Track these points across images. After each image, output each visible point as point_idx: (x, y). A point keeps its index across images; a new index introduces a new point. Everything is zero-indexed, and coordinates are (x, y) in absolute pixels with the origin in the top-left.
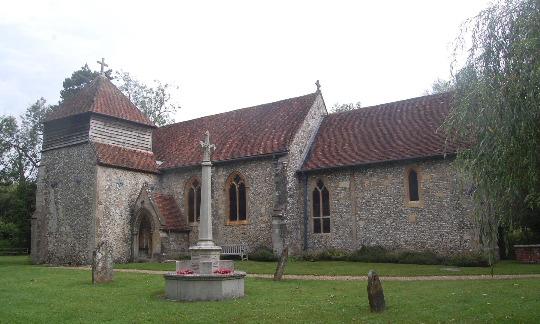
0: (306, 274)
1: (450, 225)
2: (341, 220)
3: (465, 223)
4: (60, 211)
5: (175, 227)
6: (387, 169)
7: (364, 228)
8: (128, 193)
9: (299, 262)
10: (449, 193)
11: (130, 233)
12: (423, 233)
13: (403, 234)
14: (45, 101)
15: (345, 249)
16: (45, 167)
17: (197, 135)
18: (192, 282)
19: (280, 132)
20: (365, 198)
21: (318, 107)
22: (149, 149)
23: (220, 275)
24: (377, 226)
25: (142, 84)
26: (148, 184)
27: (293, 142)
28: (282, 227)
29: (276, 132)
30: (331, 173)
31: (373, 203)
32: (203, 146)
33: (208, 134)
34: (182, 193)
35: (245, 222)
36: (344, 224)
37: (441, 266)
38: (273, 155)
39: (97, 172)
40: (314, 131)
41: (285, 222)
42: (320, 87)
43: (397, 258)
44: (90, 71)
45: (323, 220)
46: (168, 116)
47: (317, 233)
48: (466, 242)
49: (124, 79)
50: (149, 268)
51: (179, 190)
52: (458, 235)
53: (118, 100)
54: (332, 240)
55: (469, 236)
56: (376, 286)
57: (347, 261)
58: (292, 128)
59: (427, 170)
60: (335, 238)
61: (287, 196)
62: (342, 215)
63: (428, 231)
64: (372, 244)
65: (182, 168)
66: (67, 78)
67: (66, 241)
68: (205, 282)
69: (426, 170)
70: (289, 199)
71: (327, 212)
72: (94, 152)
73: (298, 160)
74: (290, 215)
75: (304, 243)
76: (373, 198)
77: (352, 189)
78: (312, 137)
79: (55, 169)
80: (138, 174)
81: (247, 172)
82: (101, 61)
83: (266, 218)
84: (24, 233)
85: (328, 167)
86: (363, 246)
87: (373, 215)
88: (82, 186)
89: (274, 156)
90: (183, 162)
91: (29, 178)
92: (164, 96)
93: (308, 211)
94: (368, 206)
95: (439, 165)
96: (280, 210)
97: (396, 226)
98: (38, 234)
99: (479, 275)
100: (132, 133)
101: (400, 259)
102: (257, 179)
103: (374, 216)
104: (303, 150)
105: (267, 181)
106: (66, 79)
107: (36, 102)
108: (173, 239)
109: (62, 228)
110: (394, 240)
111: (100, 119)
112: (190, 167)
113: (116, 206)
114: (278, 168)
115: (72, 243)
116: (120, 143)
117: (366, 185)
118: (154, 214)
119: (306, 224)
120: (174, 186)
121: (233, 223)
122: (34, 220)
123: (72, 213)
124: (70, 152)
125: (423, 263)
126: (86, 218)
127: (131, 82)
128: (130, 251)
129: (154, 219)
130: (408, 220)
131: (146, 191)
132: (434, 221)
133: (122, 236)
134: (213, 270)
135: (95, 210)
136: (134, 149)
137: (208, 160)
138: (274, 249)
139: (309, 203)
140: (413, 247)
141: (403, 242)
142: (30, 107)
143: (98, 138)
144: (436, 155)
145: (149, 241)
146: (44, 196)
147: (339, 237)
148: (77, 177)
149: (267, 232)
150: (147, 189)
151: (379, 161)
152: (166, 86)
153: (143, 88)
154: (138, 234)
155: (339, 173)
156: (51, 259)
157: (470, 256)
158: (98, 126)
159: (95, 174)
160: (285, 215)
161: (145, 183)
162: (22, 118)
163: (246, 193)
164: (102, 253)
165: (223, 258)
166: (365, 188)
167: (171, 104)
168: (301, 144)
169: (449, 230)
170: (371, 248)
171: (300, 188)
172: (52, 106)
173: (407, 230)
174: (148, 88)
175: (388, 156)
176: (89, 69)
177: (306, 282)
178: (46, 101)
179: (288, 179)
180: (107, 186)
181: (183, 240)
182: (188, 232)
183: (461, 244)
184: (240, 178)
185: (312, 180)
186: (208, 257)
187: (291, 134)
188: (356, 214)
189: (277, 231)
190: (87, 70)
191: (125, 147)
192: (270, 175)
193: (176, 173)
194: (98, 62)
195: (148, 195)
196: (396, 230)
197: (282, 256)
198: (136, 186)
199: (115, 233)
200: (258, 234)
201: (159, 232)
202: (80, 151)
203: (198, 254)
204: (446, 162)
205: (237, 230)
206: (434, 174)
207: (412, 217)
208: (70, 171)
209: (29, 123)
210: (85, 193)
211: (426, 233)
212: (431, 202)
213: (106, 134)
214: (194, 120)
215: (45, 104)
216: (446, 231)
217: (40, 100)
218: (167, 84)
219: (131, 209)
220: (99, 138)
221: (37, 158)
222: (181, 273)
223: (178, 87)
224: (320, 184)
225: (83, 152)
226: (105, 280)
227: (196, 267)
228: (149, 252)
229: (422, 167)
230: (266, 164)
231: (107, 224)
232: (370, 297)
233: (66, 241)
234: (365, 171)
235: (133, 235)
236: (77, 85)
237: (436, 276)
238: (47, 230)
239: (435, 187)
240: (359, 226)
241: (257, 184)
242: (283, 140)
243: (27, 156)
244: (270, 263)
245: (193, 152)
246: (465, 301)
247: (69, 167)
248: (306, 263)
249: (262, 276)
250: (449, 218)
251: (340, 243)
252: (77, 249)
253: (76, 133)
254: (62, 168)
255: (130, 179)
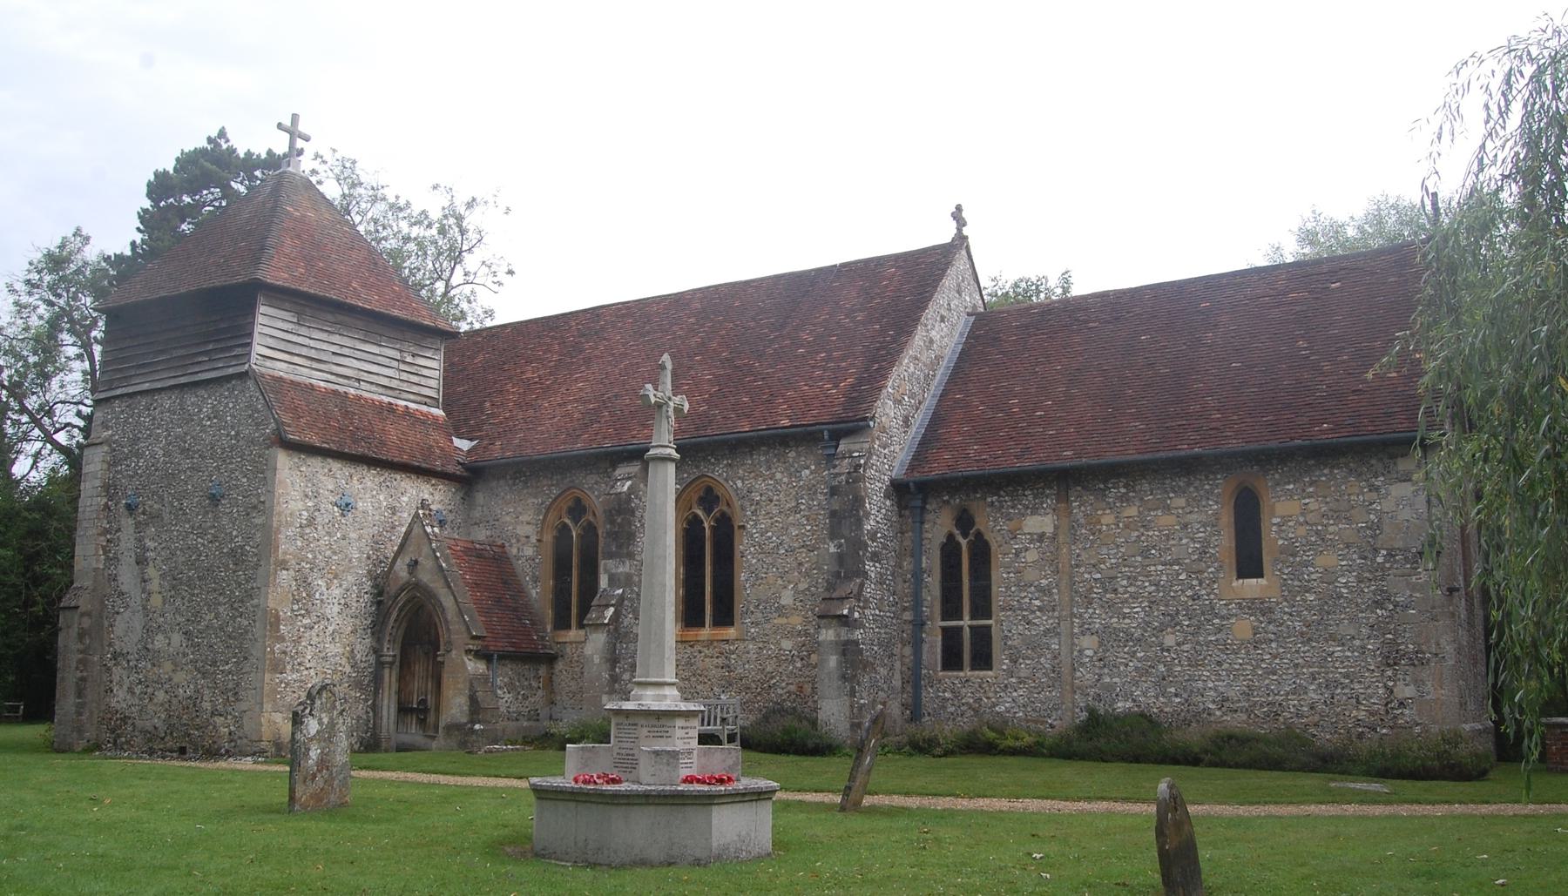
0: (928, 792)
1: (1356, 654)
2: (1027, 632)
3: (1402, 647)
4: (154, 585)
5: (513, 644)
6: (1167, 482)
7: (1095, 658)
8: (367, 537)
9: (898, 757)
10: (1355, 556)
11: (372, 659)
12: (1275, 677)
13: (1213, 678)
14: (87, 239)
15: (1036, 722)
16: (106, 448)
17: (581, 362)
18: (624, 807)
19: (843, 359)
20: (1102, 566)
21: (958, 285)
22: (434, 402)
23: (706, 788)
24: (1135, 652)
25: (397, 197)
26: (430, 510)
27: (884, 391)
28: (848, 650)
29: (829, 359)
30: (1000, 488)
31: (1125, 582)
32: (653, 402)
33: (669, 366)
34: (533, 539)
35: (731, 632)
36: (1035, 646)
37: (1331, 776)
38: (822, 432)
39: (275, 469)
40: (946, 360)
41: (858, 634)
42: (964, 225)
43: (1196, 750)
44: (234, 151)
45: (971, 632)
46: (472, 298)
47: (953, 670)
48: (1401, 704)
49: (338, 180)
50: (441, 768)
51: (522, 530)
52: (1380, 685)
53: (339, 246)
54: (996, 692)
55: (1412, 687)
56: (1179, 825)
57: (1043, 755)
58: (878, 349)
59: (1291, 486)
60: (1006, 686)
61: (864, 554)
62: (1031, 617)
63: (1291, 671)
64: (1121, 706)
65: (537, 461)
66: (161, 170)
67: (170, 679)
68: (660, 808)
69: (1287, 487)
70: (869, 566)
71: (982, 607)
72: (267, 404)
73: (897, 448)
74: (873, 615)
75: (910, 700)
76: (1125, 566)
77: (1061, 538)
78: (938, 377)
79: (138, 455)
80: (398, 477)
81: (739, 478)
82: (287, 122)
83: (796, 621)
84: (11, 652)
85: (989, 469)
86: (1092, 712)
87: (1124, 618)
88: (227, 510)
89: (826, 433)
90: (538, 445)
91: (31, 479)
92: (462, 235)
93: (925, 603)
94: (1110, 590)
95: (1326, 471)
96: (842, 599)
97: (1192, 655)
98: (80, 656)
99: (1446, 802)
100: (382, 349)
101: (1206, 752)
102: (771, 501)
103: (1127, 621)
104: (913, 417)
105: (803, 507)
106: (156, 174)
107: (58, 242)
108: (505, 680)
109: (159, 642)
110: (1185, 696)
111: (287, 305)
112: (559, 459)
113: (330, 576)
114: (836, 471)
115: (192, 687)
116: (346, 381)
117: (1104, 528)
118: (448, 602)
119: (917, 643)
120: (508, 519)
121: (692, 633)
122: (68, 613)
123: (193, 595)
124: (189, 403)
125: (1275, 765)
126: (236, 609)
127: (360, 190)
128: (371, 714)
129: (449, 618)
130: (1230, 637)
131: (425, 531)
132: (1310, 639)
133: (348, 669)
134: (684, 773)
135: (267, 585)
136: (386, 399)
137: (667, 444)
138: (821, 716)
139: (930, 579)
140: (1244, 717)
141: (1214, 702)
142: (37, 256)
143: (278, 363)
144: (1317, 442)
145: (430, 684)
146: (102, 538)
147: (1020, 683)
148: (212, 481)
149: (799, 665)
150: (427, 525)
151: (1146, 457)
152: (471, 204)
153: (401, 209)
154: (397, 663)
155: (1024, 490)
156: (119, 737)
157: (1415, 747)
158: (280, 325)
159: (269, 474)
160: (856, 615)
161: (423, 505)
162: (12, 290)
163: (736, 544)
164: (320, 719)
165: (705, 739)
166: (1101, 537)
167: (484, 262)
168: (907, 399)
169: (1352, 667)
170: (1117, 718)
171: (902, 533)
172: (109, 257)
173: (1226, 666)
174: (416, 209)
175: (1173, 443)
176: (230, 144)
177: (950, 814)
178: (64, 235)
179: (867, 505)
180: (305, 513)
181: (535, 684)
182: (551, 659)
183: (1387, 712)
184: (718, 497)
185: (941, 507)
186: (665, 734)
187: (876, 366)
188: (1073, 615)
189: (833, 661)
190: (225, 146)
191: (359, 392)
192: (812, 491)
193: (516, 478)
194: (280, 126)
195: (431, 544)
196: (1194, 664)
197: (867, 737)
198: (394, 514)
199: (325, 658)
200: (769, 669)
201: (465, 659)
202: (220, 402)
203: (636, 725)
204: (1347, 465)
205: (706, 656)
206: (1312, 500)
207: (1243, 628)
208: (187, 463)
209: (36, 308)
210: (234, 533)
211: (1284, 677)
212: (1299, 584)
213: (304, 351)
214: (571, 313)
215: (87, 249)
216: (1343, 671)
217: (70, 235)
218: (474, 200)
219: (375, 586)
220: (282, 363)
221: (55, 419)
222: (586, 782)
223: (508, 209)
224: (964, 521)
225: (231, 405)
226: (325, 801)
227: (629, 763)
228: (431, 719)
229: (1277, 476)
230: (799, 455)
231: (302, 630)
232: (1166, 860)
233: (170, 679)
234: (1102, 486)
235: (380, 664)
236: (192, 193)
237: (1321, 803)
238: (110, 645)
239: (1313, 539)
240: (1079, 651)
241: (771, 518)
242: (853, 386)
243: (23, 410)
244: (810, 758)
245: (567, 414)
246: (1430, 876)
247: (183, 451)
248: (921, 761)
249: (810, 797)
250: (1352, 632)
251: (1021, 701)
252: (207, 705)
253: (211, 347)
254: (161, 452)
255: (375, 493)
